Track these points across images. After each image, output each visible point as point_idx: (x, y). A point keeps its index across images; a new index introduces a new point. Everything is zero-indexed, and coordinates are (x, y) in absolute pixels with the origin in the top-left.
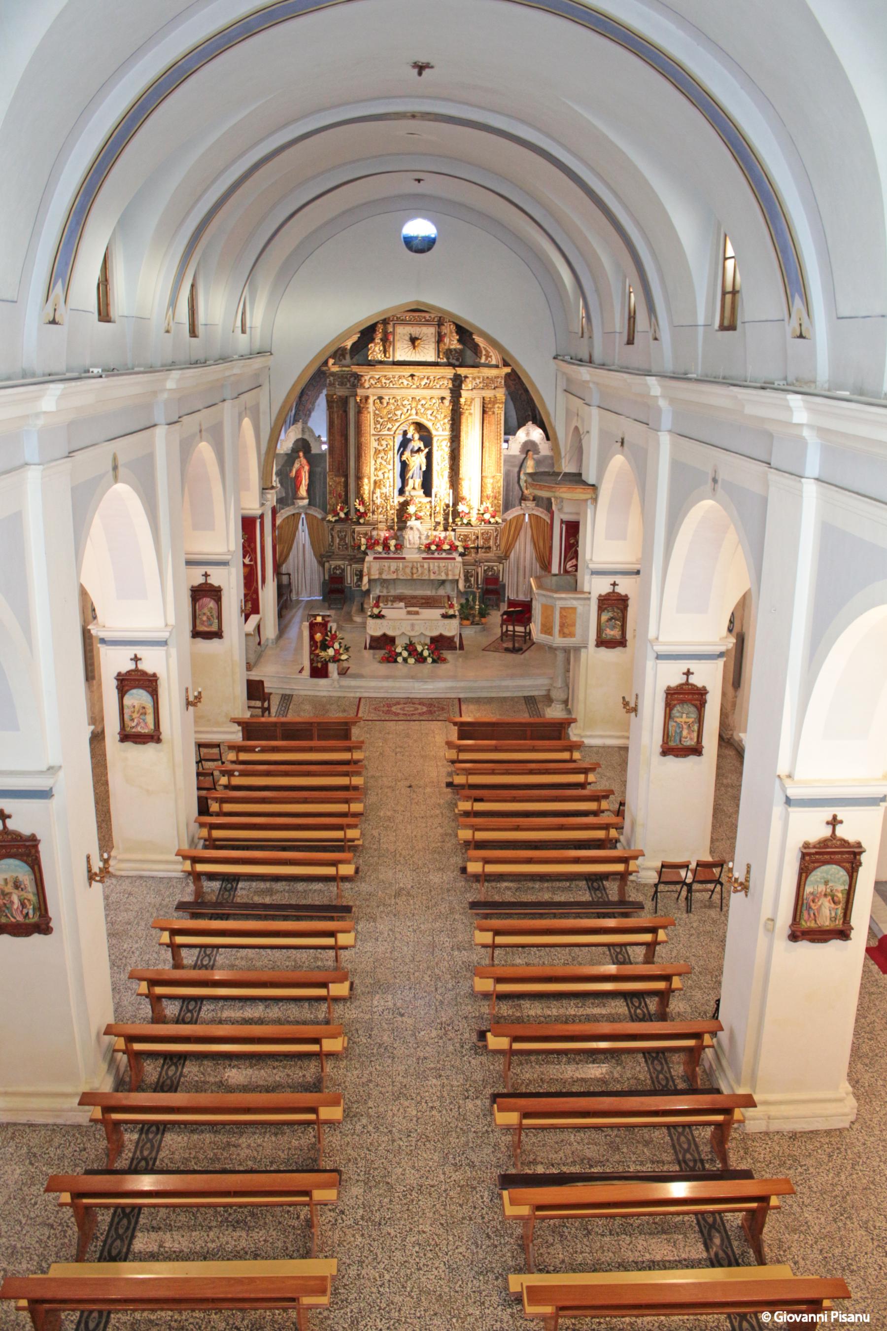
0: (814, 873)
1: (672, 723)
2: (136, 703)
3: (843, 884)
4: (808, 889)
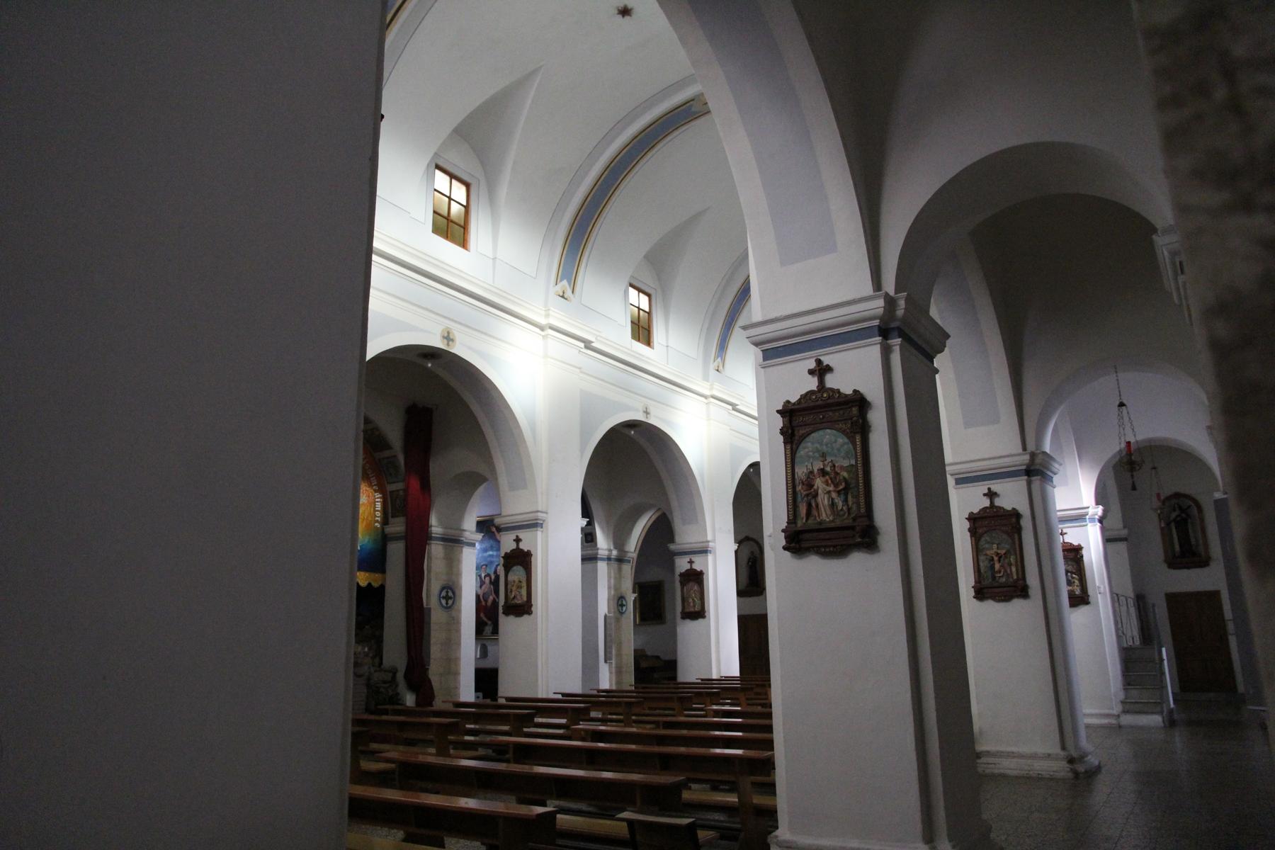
0: (803, 445)
1: (982, 558)
2: (516, 578)
3: (847, 456)
4: (801, 471)
